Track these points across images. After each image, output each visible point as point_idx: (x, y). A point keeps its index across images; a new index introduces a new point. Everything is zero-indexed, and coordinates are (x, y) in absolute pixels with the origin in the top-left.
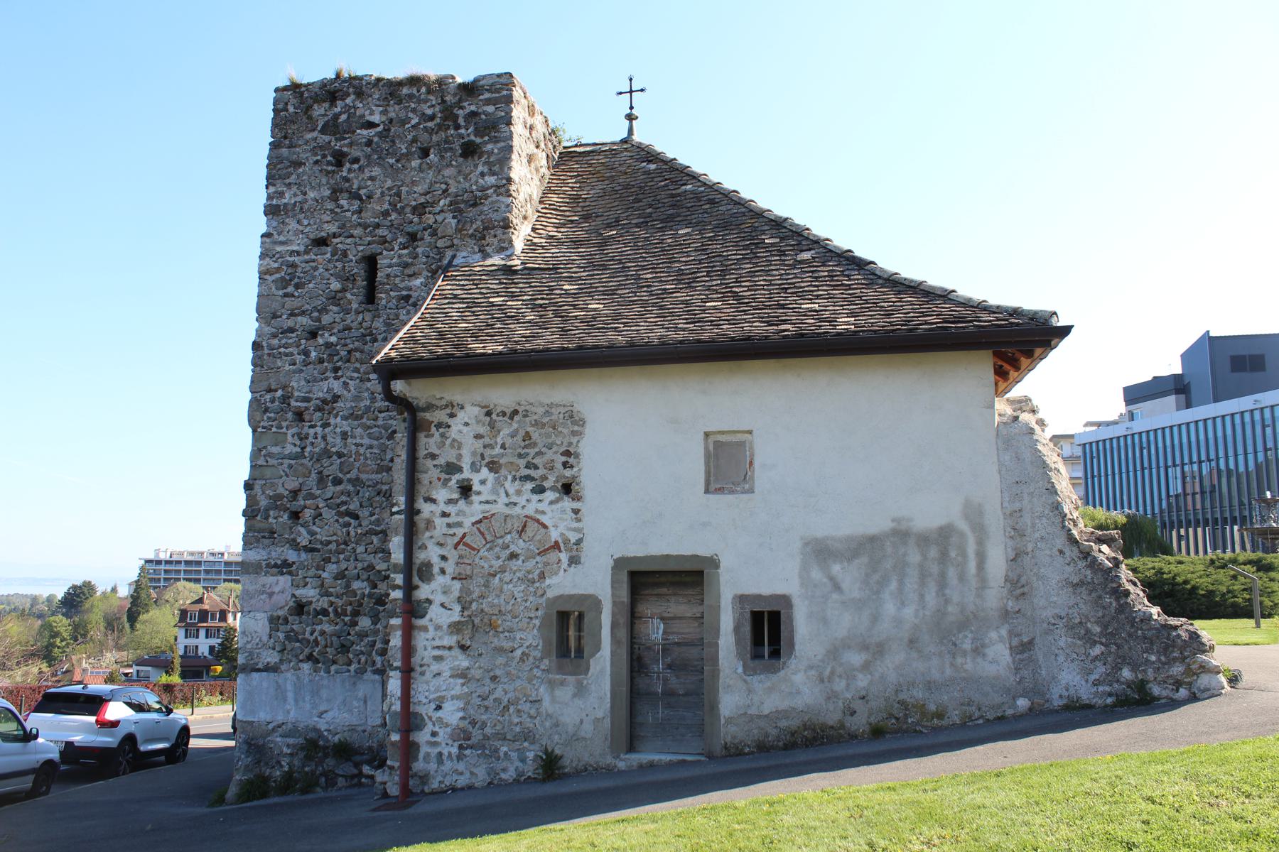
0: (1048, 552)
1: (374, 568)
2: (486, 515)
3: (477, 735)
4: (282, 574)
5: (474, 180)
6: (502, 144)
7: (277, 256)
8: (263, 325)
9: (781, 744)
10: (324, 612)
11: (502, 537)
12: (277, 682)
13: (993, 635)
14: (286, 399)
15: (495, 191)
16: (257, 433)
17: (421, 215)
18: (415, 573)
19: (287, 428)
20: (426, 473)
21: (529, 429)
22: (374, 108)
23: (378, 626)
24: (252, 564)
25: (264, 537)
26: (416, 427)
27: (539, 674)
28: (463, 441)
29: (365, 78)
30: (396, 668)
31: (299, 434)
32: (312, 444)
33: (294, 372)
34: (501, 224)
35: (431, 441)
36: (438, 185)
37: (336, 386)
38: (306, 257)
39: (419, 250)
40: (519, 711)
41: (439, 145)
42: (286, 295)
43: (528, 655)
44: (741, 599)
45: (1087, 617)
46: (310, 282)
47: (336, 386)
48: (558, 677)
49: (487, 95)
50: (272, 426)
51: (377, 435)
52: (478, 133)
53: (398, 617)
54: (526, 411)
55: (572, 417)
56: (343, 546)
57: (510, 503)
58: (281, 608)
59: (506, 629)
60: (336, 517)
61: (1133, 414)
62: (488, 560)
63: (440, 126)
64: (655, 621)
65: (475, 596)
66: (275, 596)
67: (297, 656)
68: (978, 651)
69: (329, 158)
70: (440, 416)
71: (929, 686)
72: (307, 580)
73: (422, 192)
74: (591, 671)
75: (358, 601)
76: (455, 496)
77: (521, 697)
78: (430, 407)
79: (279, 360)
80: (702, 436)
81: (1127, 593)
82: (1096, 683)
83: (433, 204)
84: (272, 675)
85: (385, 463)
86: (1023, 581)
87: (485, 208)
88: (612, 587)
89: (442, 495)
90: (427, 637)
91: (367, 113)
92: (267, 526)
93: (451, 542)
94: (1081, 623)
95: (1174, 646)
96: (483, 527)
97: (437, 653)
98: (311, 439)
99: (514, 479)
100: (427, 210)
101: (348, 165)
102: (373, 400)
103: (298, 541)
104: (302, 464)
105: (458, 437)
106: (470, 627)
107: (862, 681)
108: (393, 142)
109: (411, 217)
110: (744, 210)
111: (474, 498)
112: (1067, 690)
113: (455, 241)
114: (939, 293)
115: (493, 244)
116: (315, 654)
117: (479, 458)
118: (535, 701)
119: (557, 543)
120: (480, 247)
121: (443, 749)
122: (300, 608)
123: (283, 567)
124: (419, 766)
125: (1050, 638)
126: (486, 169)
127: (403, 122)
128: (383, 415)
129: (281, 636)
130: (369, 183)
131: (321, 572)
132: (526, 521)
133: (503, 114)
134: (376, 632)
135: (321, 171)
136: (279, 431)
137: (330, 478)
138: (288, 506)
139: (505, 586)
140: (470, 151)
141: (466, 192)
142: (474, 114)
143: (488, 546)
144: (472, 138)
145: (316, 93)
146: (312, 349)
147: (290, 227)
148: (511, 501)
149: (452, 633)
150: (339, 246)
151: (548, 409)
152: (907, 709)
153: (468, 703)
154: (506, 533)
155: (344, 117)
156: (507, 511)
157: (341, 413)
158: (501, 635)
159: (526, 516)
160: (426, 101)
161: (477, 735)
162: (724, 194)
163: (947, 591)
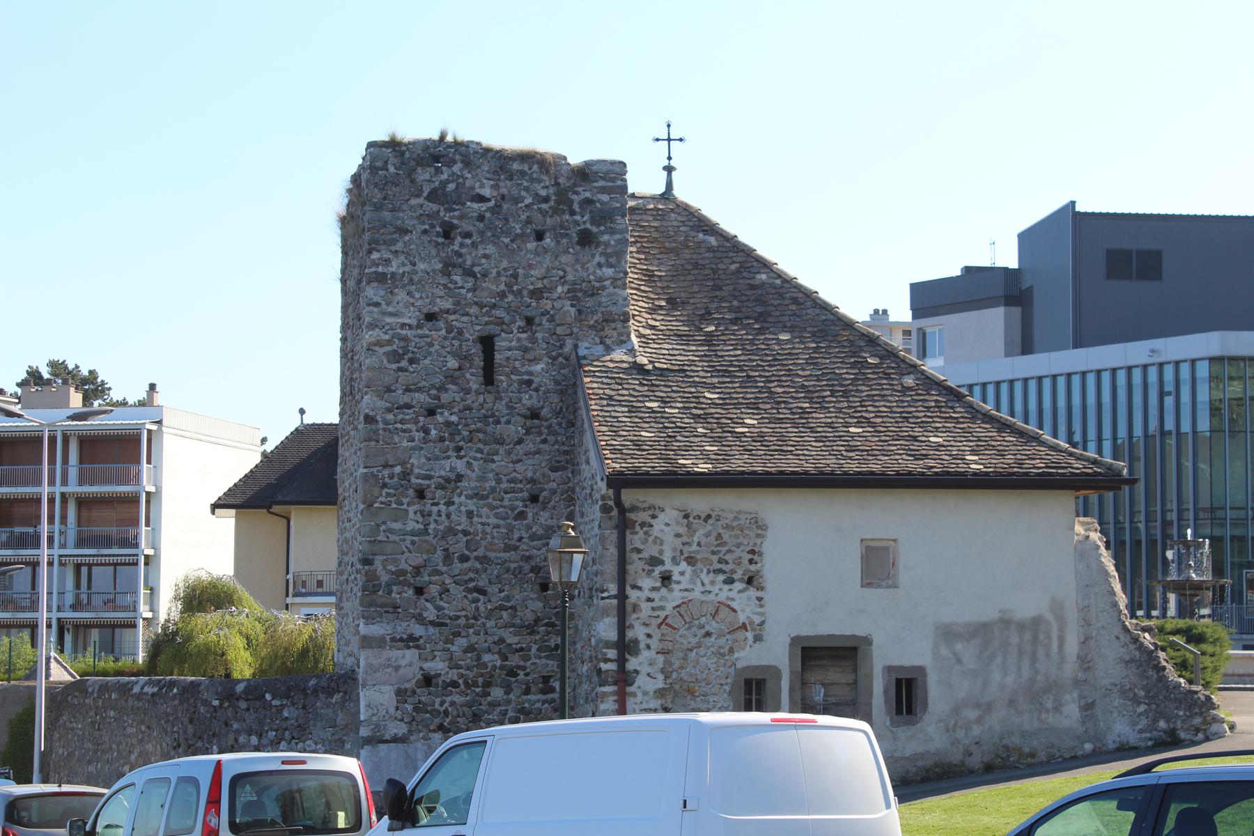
0: (1107, 637)
1: (504, 641)
4: (409, 647)
5: (591, 270)
6: (618, 236)
8: (375, 399)
9: (919, 778)
10: (454, 684)
12: (406, 752)
13: (1068, 697)
14: (405, 475)
15: (612, 283)
17: (538, 299)
19: (409, 505)
20: (632, 564)
21: (722, 531)
22: (485, 181)
23: (511, 696)
24: (376, 638)
28: (664, 538)
29: (470, 145)
32: (436, 521)
33: (413, 449)
34: (622, 318)
35: (636, 537)
36: (555, 271)
37: (460, 465)
41: (554, 229)
42: (400, 369)
44: (889, 669)
45: (1135, 685)
46: (425, 358)
49: (601, 183)
50: (391, 502)
52: (594, 221)
53: (609, 685)
54: (719, 516)
55: (756, 522)
56: (472, 621)
57: (706, 591)
58: (408, 681)
59: (702, 693)
60: (464, 594)
61: (924, 334)
62: (687, 637)
63: (555, 211)
64: (817, 686)
65: (674, 667)
67: (427, 726)
68: (1057, 709)
69: (438, 229)
70: (643, 516)
71: (1023, 734)
73: (539, 276)
75: (490, 672)
76: (658, 584)
78: (634, 509)
79: (396, 436)
81: (1164, 668)
82: (1141, 731)
83: (550, 290)
84: (401, 745)
85: (513, 542)
86: (1089, 658)
87: (604, 300)
88: (790, 660)
89: (646, 583)
90: (636, 701)
91: (477, 184)
93: (655, 622)
94: (1130, 689)
95: (1195, 705)
96: (682, 610)
98: (434, 517)
99: (709, 572)
102: (499, 481)
103: (425, 616)
104: (426, 541)
105: (659, 535)
106: (672, 692)
107: (976, 731)
108: (507, 220)
109: (529, 301)
110: (832, 317)
111: (674, 586)
112: (1119, 737)
113: (575, 330)
114: (1032, 435)
115: (612, 337)
116: (445, 724)
117: (678, 553)
119: (744, 624)
120: (601, 338)
122: (428, 680)
123: (410, 641)
125: (1107, 700)
126: (603, 260)
127: (517, 200)
128: (509, 496)
129: (409, 708)
130: (484, 261)
131: (450, 646)
133: (618, 205)
134: (509, 702)
137: (456, 555)
138: (412, 581)
139: (701, 659)
140: (586, 239)
141: (584, 281)
142: (588, 201)
143: (687, 626)
144: (588, 226)
145: (419, 155)
146: (432, 427)
147: (399, 298)
149: (657, 697)
150: (454, 323)
151: (736, 515)
152: (1009, 751)
155: (451, 186)
156: (703, 598)
157: (465, 493)
158: (698, 699)
159: (719, 602)
160: (540, 181)
162: (805, 294)
163: (1037, 665)
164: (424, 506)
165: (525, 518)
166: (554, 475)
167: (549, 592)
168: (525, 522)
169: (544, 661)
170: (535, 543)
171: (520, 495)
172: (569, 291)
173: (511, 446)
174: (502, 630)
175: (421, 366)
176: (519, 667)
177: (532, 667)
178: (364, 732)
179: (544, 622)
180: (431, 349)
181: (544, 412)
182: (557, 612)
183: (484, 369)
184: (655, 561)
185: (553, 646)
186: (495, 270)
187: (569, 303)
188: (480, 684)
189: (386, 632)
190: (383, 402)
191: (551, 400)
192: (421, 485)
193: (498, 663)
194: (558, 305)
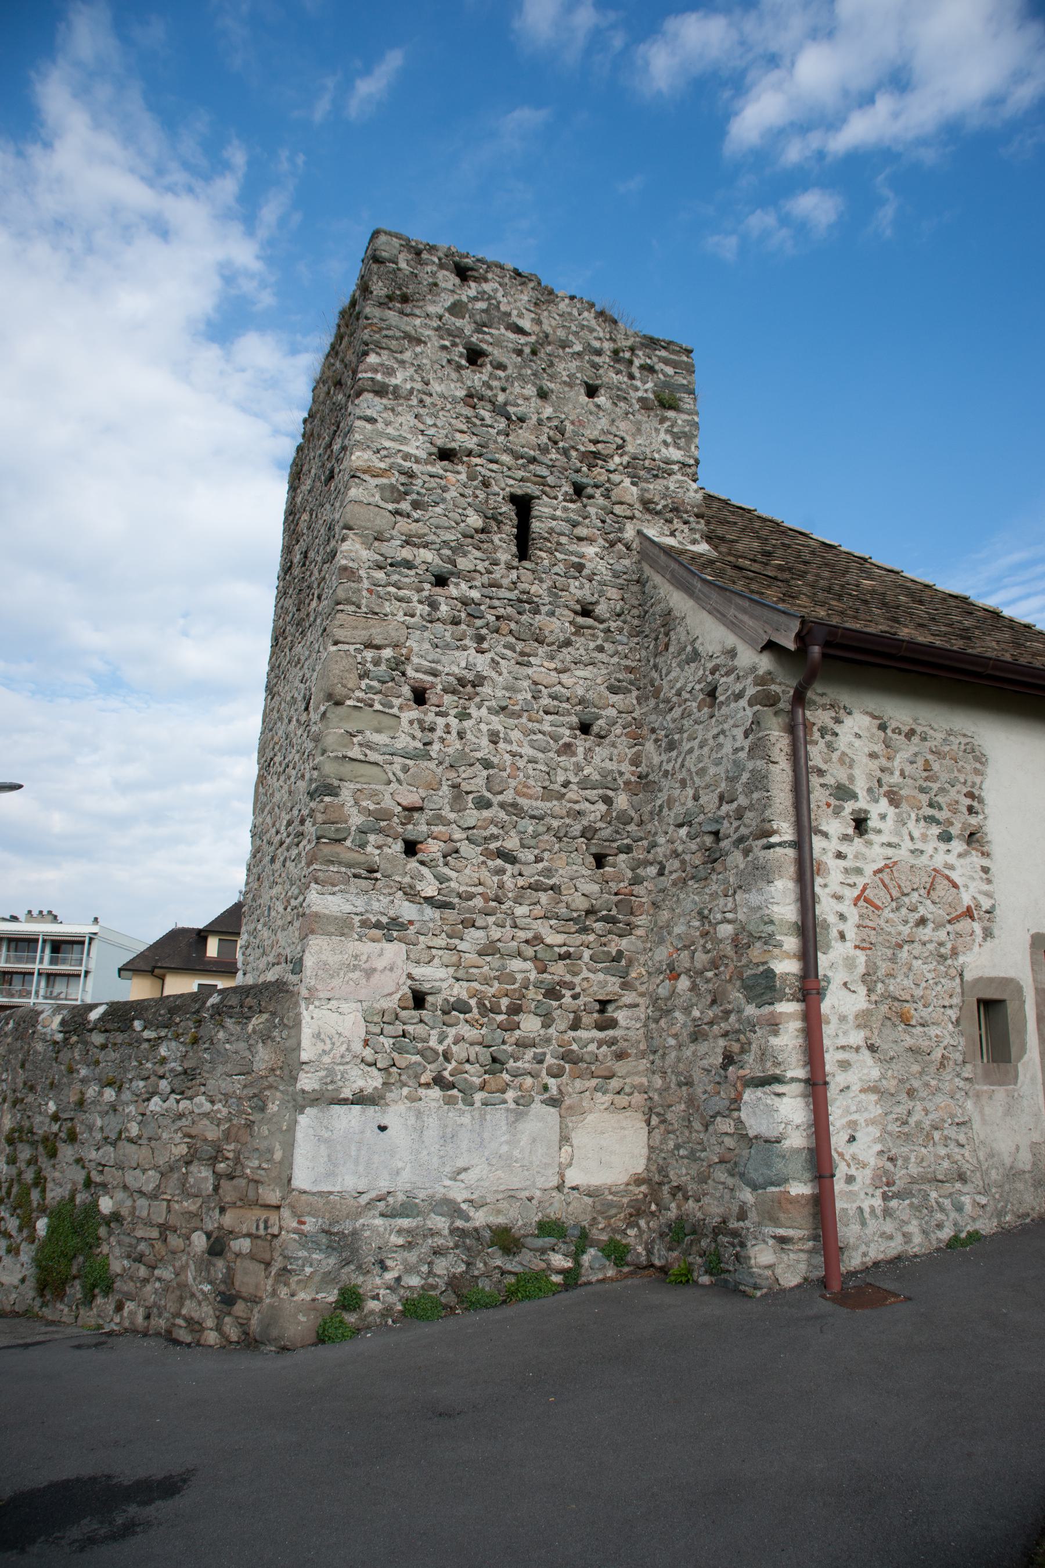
2: (888, 862)
7: (384, 453)
10: (462, 1007)
14: (398, 665)
19: (400, 708)
21: (930, 757)
22: (524, 311)
23: (551, 1031)
25: (355, 876)
27: (962, 1084)
31: (420, 722)
32: (442, 740)
37: (482, 663)
40: (947, 1138)
42: (397, 513)
48: (985, 1088)
51: (544, 745)
53: (788, 1000)
56: (494, 904)
57: (917, 850)
60: (482, 858)
66: (376, 976)
69: (461, 349)
74: (1021, 1078)
76: (850, 831)
77: (946, 1117)
79: (387, 603)
84: (371, 1110)
85: (556, 787)
92: (361, 858)
93: (851, 894)
96: (885, 876)
98: (439, 732)
103: (419, 888)
105: (848, 751)
109: (579, 465)
111: (871, 836)
116: (446, 1074)
118: (964, 1123)
119: (969, 908)
121: (862, 1201)
126: (669, 439)
131: (457, 941)
132: (935, 877)
133: (685, 382)
134: (548, 1041)
136: (387, 710)
137: (471, 796)
143: (894, 904)
146: (442, 600)
148: (917, 847)
149: (858, 1026)
150: (478, 468)
153: (884, 1130)
154: (913, 890)
155: (481, 305)
156: (913, 861)
157: (486, 703)
159: (934, 870)
164: (425, 714)
165: (574, 754)
166: (614, 699)
167: (607, 869)
168: (574, 759)
169: (601, 976)
170: (588, 792)
171: (567, 719)
173: (555, 647)
174: (539, 921)
177: (585, 984)
179: (600, 914)
180: (445, 495)
181: (601, 609)
182: (620, 901)
183: (517, 537)
184: (843, 793)
185: (614, 954)
188: (504, 1009)
189: (354, 910)
191: (609, 595)
193: (533, 976)
194: (616, 478)
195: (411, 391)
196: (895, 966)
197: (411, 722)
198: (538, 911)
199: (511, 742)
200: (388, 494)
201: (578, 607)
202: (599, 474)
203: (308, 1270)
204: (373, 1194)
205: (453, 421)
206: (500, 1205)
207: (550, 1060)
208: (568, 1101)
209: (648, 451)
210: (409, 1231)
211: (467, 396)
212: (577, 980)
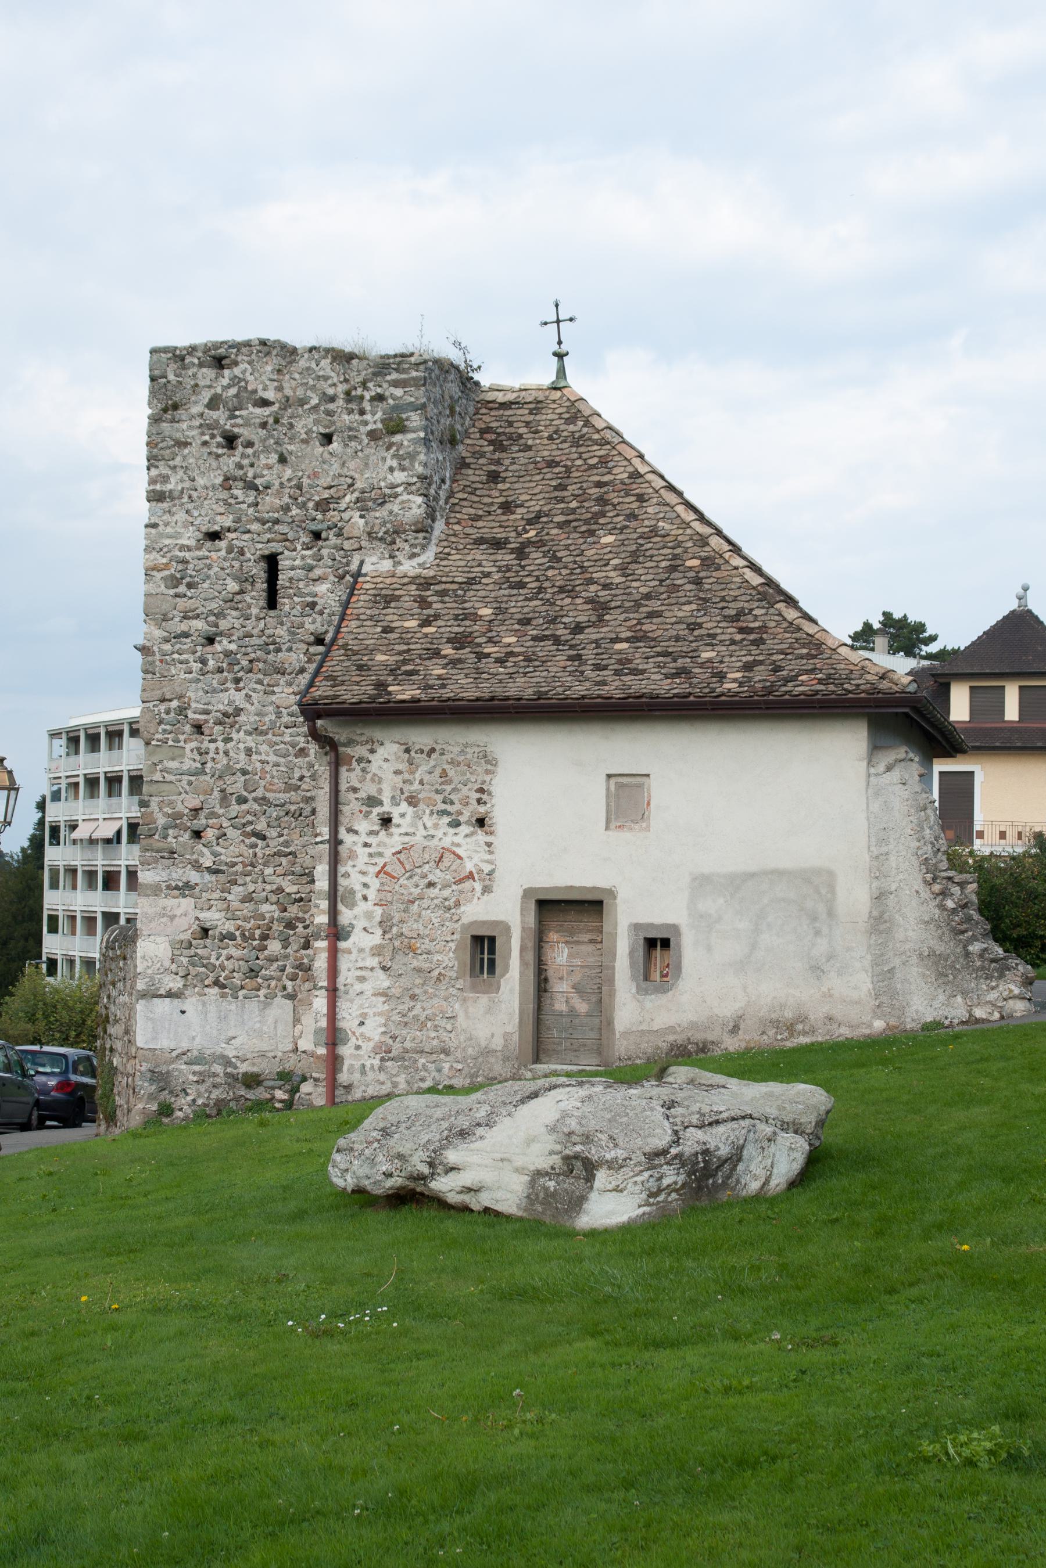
3: (397, 1049)
7: (165, 550)
10: (231, 937)
11: (420, 867)
14: (182, 711)
15: (406, 488)
16: (150, 747)
17: (325, 511)
18: (339, 899)
19: (185, 741)
21: (446, 766)
22: (268, 383)
23: (288, 950)
25: (162, 857)
26: (337, 763)
27: (454, 992)
28: (383, 776)
30: (321, 988)
31: (198, 749)
32: (214, 759)
35: (353, 775)
36: (342, 479)
37: (239, 698)
38: (200, 553)
39: (325, 552)
40: (436, 1026)
42: (177, 596)
43: (444, 976)
44: (636, 927)
47: (239, 698)
50: (168, 739)
55: (485, 756)
56: (249, 868)
60: (242, 838)
65: (395, 921)
66: (177, 919)
69: (219, 439)
72: (212, 902)
74: (502, 988)
76: (376, 828)
80: (604, 777)
83: (338, 500)
85: (294, 782)
86: (886, 916)
89: (363, 826)
91: (260, 387)
92: (165, 846)
96: (402, 857)
97: (360, 973)
98: (212, 754)
99: (432, 813)
100: (331, 506)
101: (240, 448)
102: (279, 715)
105: (378, 772)
109: (314, 513)
111: (393, 830)
116: (221, 979)
117: (399, 792)
119: (471, 873)
123: (186, 889)
124: (343, 1077)
126: (395, 463)
129: (185, 960)
131: (226, 895)
134: (286, 957)
135: (210, 453)
137: (234, 796)
139: (423, 912)
142: (380, 398)
143: (408, 875)
146: (209, 656)
147: (176, 517)
150: (234, 542)
153: (388, 1019)
155: (233, 391)
161: (397, 1049)
164: (202, 743)
165: (307, 755)
168: (307, 759)
172: (358, 500)
175: (200, 590)
176: (298, 919)
178: (141, 985)
184: (373, 801)
186: (278, 481)
187: (358, 513)
188: (257, 937)
190: (160, 631)
192: (198, 720)
195: (182, 492)
196: (406, 915)
197: (192, 751)
198: (280, 870)
199: (260, 754)
200: (169, 583)
201: (312, 639)
202: (333, 516)
203: (142, 1092)
204: (179, 1051)
205: (214, 507)
206: (255, 1060)
207: (289, 970)
208: (300, 996)
209: (375, 482)
210: (200, 1073)
211: (224, 480)
212: (307, 916)
